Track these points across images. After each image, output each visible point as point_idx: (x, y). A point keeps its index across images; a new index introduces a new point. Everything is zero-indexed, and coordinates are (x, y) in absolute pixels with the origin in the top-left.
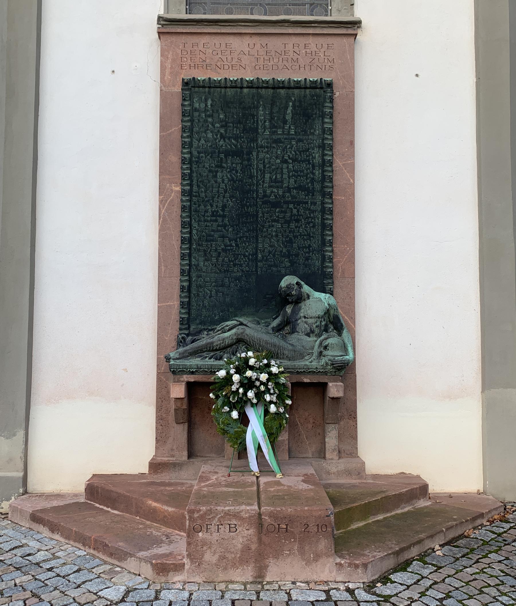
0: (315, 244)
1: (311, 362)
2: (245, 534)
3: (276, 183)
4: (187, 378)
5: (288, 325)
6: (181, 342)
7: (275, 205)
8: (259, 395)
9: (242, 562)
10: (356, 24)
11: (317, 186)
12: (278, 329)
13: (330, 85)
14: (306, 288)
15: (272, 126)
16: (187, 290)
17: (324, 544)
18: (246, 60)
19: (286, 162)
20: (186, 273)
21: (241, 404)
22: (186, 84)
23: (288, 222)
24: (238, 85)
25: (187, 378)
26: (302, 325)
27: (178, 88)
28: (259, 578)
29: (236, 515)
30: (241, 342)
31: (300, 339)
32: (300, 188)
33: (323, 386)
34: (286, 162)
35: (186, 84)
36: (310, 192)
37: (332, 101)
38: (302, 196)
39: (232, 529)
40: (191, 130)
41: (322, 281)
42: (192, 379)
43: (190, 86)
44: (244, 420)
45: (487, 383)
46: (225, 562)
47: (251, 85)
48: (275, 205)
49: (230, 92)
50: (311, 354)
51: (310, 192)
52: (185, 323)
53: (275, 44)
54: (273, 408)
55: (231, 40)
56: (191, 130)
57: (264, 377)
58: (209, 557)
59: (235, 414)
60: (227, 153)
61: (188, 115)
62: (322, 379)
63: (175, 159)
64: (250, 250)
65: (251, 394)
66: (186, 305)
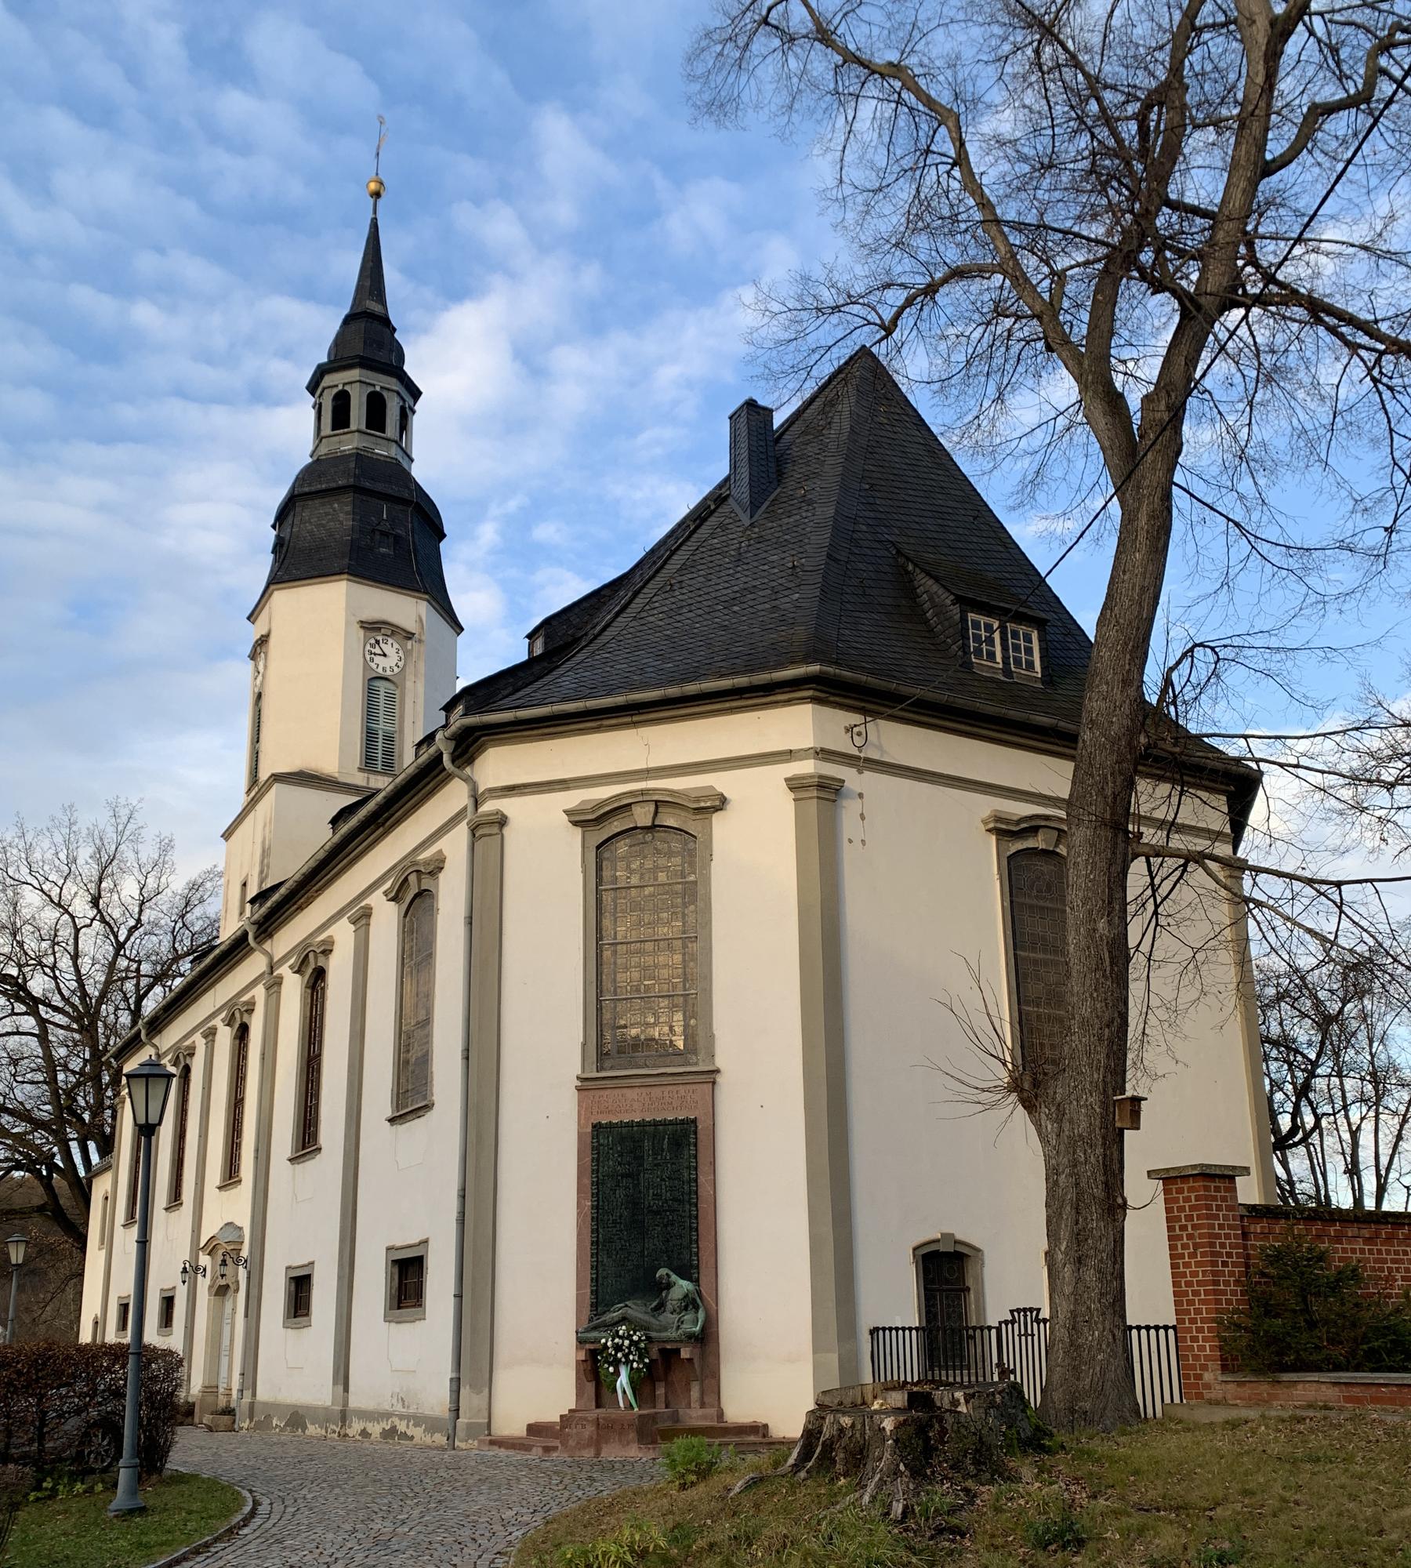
0: (685, 1242)
1: (672, 1334)
2: (590, 1429)
3: (657, 1196)
4: (588, 1346)
5: (661, 1307)
6: (591, 1320)
7: (657, 1213)
8: (626, 1356)
9: (588, 1446)
10: (718, 1071)
11: (686, 1198)
12: (656, 1309)
13: (694, 1121)
14: (674, 1277)
15: (654, 1154)
16: (595, 1281)
17: (632, 1435)
18: (636, 1105)
19: (663, 1180)
20: (595, 1267)
21: (616, 1363)
22: (594, 1126)
23: (666, 1226)
24: (630, 1125)
25: (588, 1346)
26: (669, 1307)
27: (590, 1129)
28: (597, 1455)
29: (585, 1419)
30: (623, 1320)
31: (668, 1317)
32: (674, 1200)
33: (678, 1351)
34: (663, 1180)
35: (594, 1126)
36: (681, 1202)
37: (695, 1133)
38: (676, 1205)
39: (584, 1427)
40: (598, 1160)
41: (689, 1271)
42: (592, 1347)
43: (597, 1127)
44: (617, 1373)
45: (814, 1352)
46: (580, 1446)
47: (639, 1124)
48: (657, 1213)
49: (624, 1130)
50: (675, 1326)
51: (681, 1202)
52: (594, 1306)
53: (656, 1092)
54: (635, 1365)
55: (625, 1091)
56: (598, 1160)
57: (627, 1343)
58: (571, 1443)
59: (611, 1369)
60: (623, 1176)
61: (596, 1149)
62: (678, 1345)
63: (587, 1182)
64: (639, 1248)
65: (619, 1355)
66: (595, 1293)
